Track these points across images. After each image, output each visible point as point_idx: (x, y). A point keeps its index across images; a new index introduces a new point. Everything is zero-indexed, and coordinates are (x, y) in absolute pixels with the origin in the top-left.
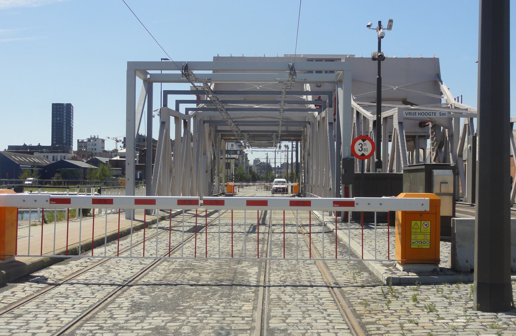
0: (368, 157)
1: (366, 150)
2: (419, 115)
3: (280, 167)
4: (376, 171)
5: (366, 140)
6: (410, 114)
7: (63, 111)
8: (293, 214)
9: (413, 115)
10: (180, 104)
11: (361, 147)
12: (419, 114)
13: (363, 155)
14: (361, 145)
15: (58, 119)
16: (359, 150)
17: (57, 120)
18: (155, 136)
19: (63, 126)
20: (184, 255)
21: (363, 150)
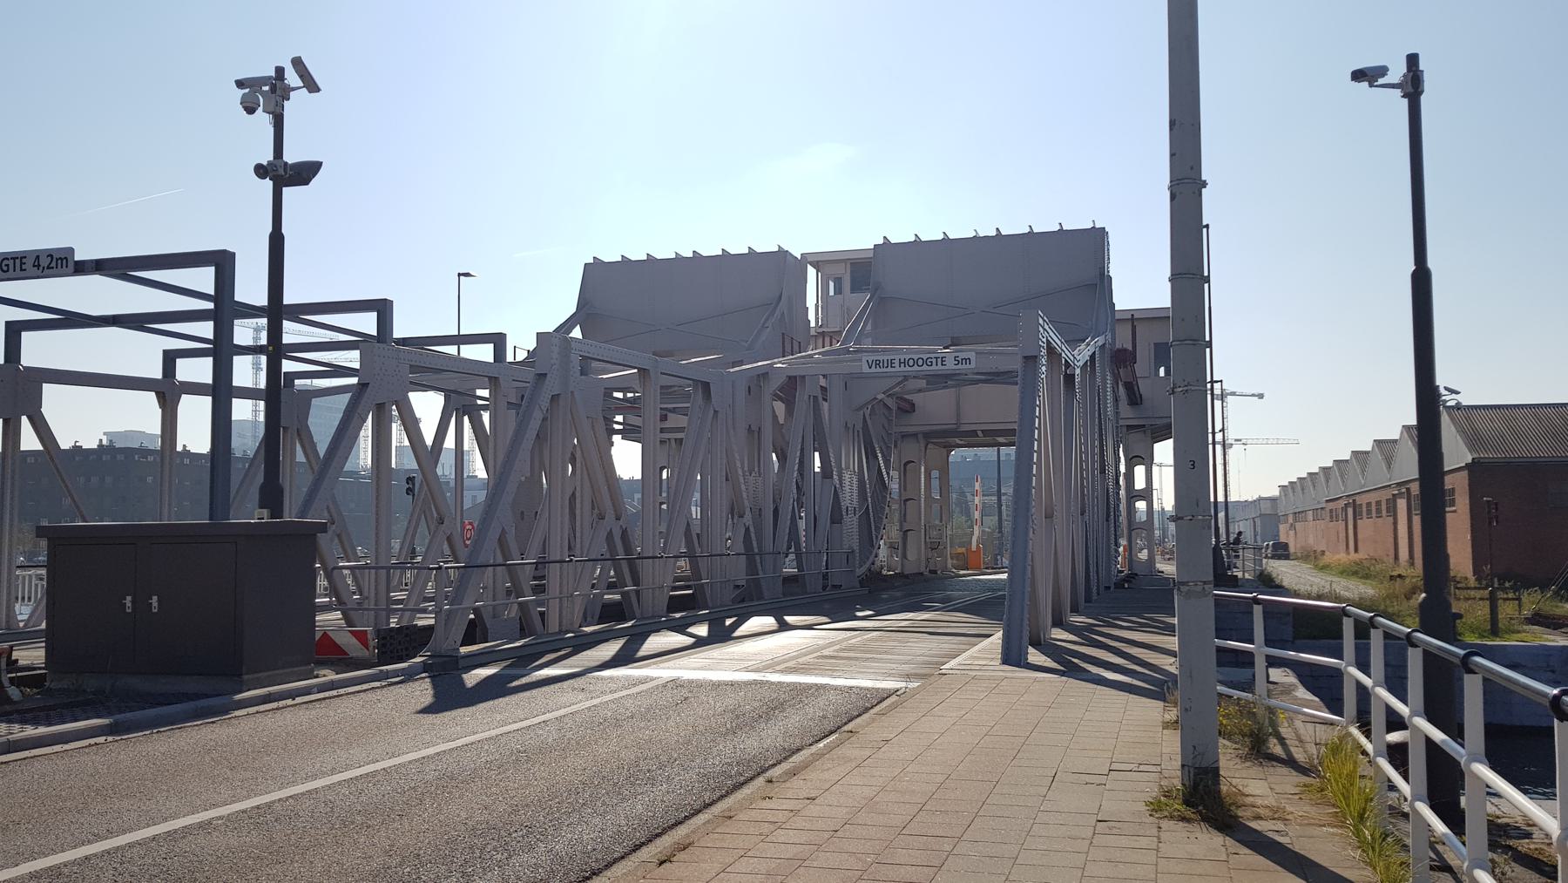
2: (902, 365)
6: (877, 363)
8: (542, 416)
9: (886, 365)
12: (900, 363)
20: (646, 568)
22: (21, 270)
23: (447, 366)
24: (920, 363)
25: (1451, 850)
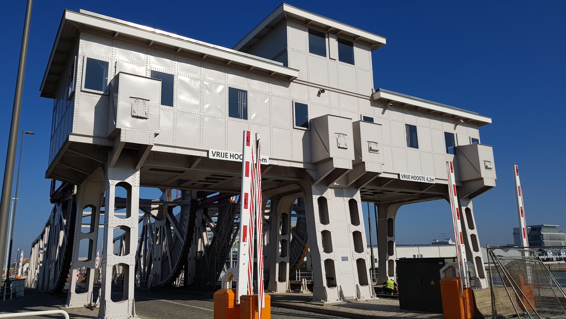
2: (232, 157)
9: (223, 156)
10: (161, 82)
12: (231, 156)
18: (157, 206)
22: (226, 157)
23: (89, 235)
24: (237, 157)
25: (303, 191)
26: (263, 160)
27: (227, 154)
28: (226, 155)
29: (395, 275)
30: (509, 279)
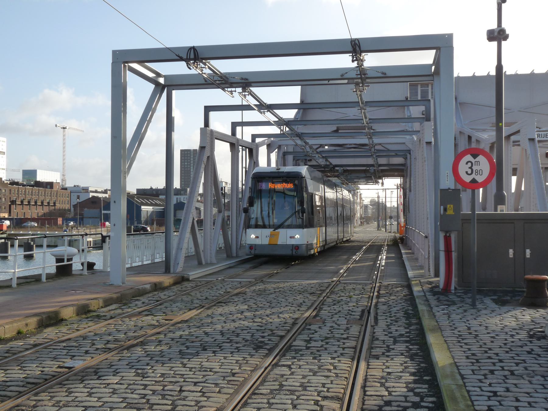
0: (484, 184)
1: (478, 172)
3: (103, 191)
4: (496, 210)
5: (479, 155)
7: (190, 157)
9: (543, 136)
11: (471, 168)
13: (474, 181)
14: (470, 164)
15: (186, 163)
16: (467, 172)
17: (185, 165)
19: (190, 170)
21: (474, 172)
22: (546, 137)
26: (476, 162)
27: (547, 135)
28: (546, 136)
29: (469, 148)
30: (234, 279)
